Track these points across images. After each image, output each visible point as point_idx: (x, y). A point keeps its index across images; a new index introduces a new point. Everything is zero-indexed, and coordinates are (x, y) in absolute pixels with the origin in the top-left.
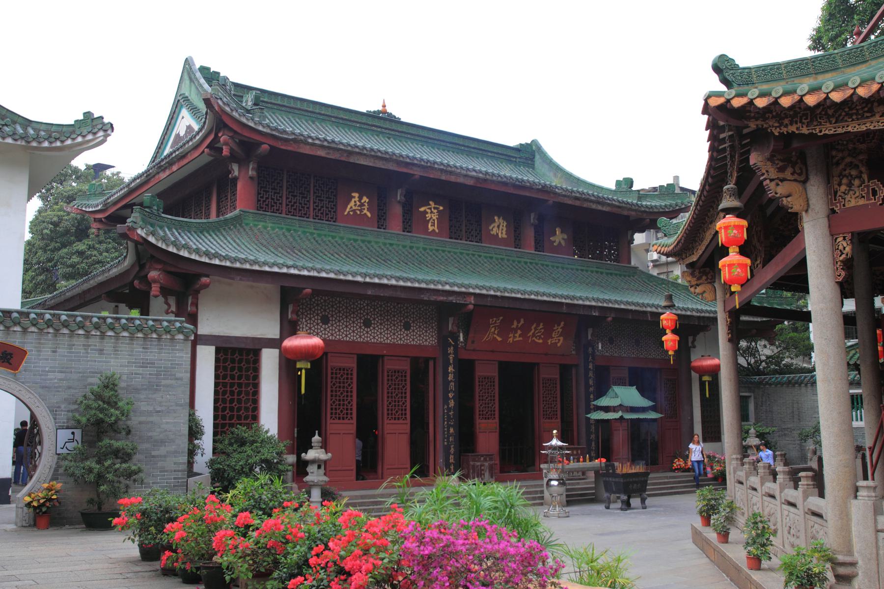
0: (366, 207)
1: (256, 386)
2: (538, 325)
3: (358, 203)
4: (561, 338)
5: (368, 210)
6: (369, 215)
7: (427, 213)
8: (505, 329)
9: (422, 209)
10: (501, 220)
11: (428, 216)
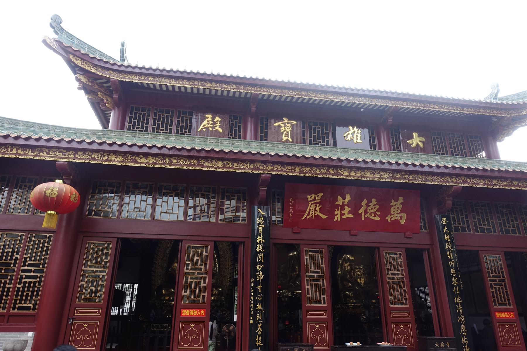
2: (370, 201)
3: (211, 122)
6: (220, 130)
9: (277, 124)
10: (356, 129)
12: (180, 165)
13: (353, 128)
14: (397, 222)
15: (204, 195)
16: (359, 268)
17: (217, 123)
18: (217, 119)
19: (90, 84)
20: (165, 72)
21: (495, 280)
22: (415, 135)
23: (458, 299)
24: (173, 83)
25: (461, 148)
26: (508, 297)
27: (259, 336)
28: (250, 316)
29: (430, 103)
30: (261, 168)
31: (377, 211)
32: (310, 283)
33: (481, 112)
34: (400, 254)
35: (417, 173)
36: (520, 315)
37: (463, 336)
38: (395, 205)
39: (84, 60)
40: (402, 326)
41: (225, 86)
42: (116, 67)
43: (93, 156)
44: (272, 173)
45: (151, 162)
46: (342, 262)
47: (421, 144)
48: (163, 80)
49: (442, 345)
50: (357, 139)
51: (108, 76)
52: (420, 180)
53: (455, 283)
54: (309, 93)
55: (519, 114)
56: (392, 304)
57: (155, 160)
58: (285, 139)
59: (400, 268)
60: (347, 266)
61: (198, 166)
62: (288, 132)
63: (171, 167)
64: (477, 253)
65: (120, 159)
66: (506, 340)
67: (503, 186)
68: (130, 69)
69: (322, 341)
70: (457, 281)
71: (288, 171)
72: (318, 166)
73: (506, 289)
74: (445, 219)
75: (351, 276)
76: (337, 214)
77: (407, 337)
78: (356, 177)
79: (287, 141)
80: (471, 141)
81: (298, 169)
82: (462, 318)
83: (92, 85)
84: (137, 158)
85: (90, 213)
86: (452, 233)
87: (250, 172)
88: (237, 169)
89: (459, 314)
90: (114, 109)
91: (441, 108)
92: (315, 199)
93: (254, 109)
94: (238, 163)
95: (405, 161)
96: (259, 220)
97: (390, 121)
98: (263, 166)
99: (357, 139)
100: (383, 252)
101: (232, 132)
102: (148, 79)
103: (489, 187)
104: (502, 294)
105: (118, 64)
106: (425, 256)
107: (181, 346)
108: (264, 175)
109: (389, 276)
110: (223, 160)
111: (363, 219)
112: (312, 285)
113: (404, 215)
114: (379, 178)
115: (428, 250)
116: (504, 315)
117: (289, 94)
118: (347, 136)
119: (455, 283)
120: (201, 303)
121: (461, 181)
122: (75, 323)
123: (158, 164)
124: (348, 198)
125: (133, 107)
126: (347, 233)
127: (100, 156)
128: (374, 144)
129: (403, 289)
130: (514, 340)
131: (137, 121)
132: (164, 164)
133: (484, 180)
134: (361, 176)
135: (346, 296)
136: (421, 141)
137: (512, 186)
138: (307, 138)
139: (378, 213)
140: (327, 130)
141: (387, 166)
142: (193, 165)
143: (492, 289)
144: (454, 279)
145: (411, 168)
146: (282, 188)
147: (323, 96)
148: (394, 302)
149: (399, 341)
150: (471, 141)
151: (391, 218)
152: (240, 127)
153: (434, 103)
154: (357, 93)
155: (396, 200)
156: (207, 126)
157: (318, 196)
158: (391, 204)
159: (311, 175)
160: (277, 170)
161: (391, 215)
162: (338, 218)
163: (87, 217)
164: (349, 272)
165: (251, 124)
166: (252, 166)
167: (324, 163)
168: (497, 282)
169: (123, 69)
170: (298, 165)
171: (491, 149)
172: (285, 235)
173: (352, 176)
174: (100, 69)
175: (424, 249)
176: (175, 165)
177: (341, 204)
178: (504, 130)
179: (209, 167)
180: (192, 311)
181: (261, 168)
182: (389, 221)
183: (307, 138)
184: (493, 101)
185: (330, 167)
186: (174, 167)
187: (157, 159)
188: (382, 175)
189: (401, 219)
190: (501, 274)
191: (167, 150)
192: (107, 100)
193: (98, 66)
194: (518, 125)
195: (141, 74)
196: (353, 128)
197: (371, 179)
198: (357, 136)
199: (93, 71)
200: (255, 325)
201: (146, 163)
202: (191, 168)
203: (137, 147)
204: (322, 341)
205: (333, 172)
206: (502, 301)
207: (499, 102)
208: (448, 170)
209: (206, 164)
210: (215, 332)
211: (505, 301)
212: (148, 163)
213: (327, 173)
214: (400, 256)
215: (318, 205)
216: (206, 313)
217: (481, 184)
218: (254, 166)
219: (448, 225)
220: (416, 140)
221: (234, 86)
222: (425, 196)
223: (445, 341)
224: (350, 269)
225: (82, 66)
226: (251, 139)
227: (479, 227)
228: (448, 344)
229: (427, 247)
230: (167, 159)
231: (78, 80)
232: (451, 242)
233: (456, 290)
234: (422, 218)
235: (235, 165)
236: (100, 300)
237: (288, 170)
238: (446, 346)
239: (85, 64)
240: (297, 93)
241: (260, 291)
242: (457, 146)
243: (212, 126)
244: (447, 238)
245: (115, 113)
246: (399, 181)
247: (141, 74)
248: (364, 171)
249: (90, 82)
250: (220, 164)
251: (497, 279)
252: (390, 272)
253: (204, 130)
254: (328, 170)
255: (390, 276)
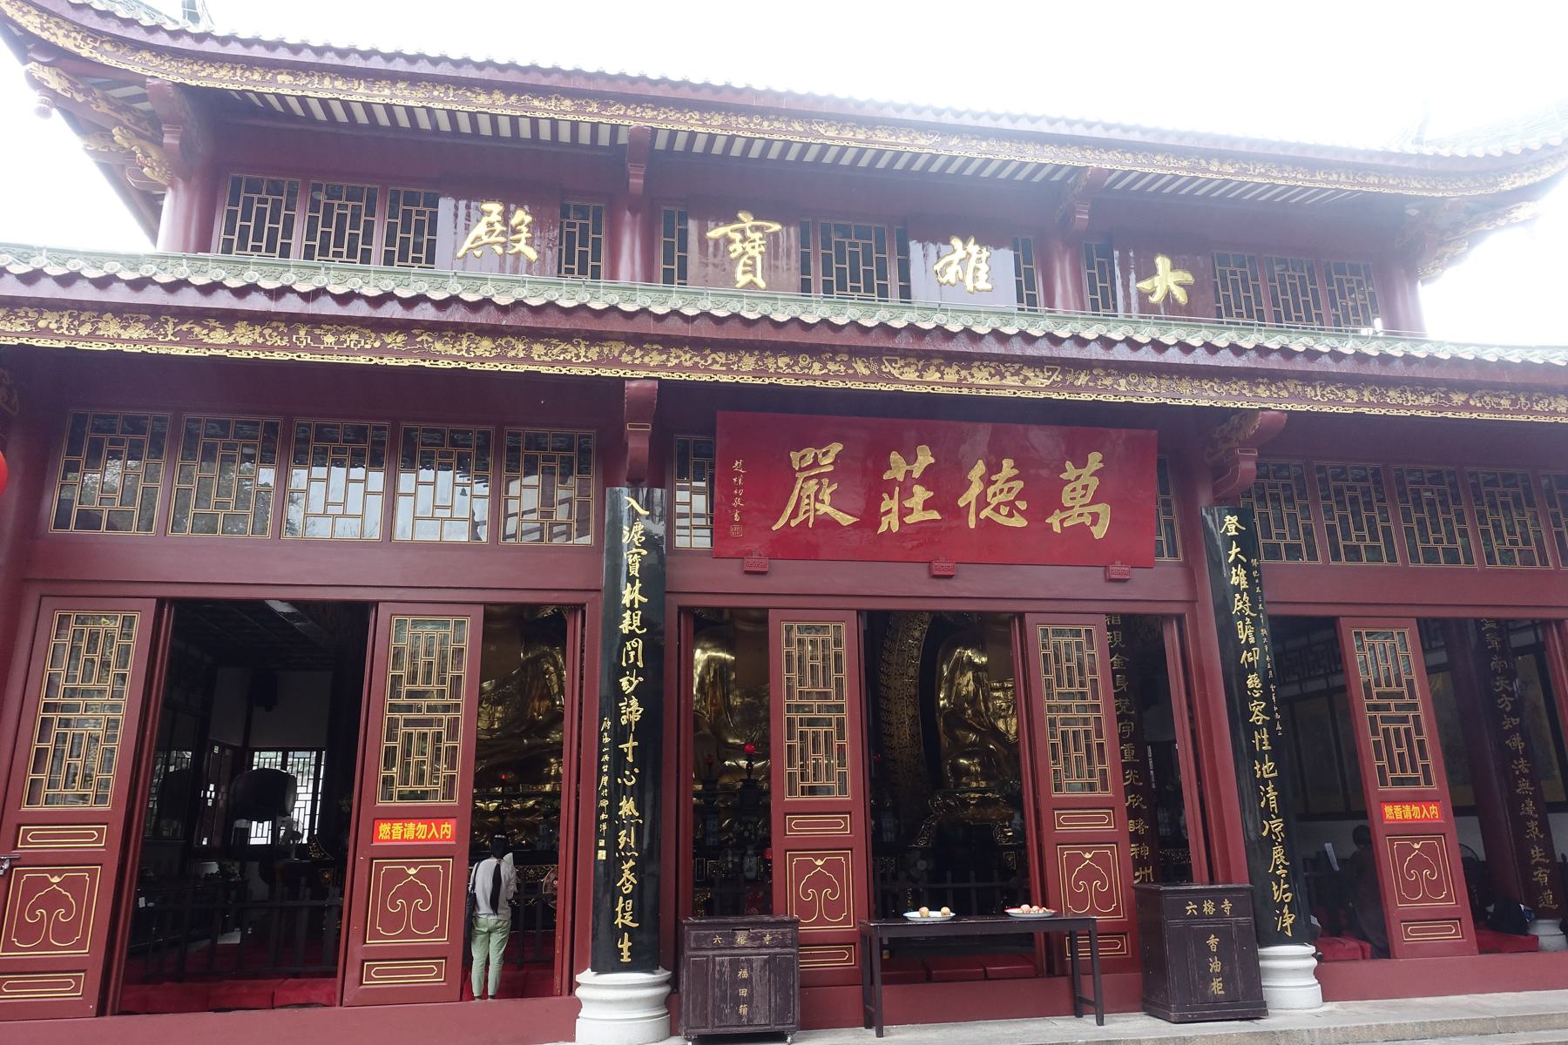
0: (525, 234)
1: (970, 613)
2: (994, 468)
3: (499, 228)
4: (1103, 509)
5: (530, 242)
6: (532, 254)
7: (729, 241)
8: (865, 479)
10: (973, 247)
11: (736, 248)
12: (348, 351)
13: (965, 241)
14: (1082, 531)
15: (450, 455)
16: (1003, 689)
17: (519, 232)
18: (521, 217)
19: (80, 98)
20: (329, 55)
21: (1387, 708)
22: (1162, 263)
23: (1267, 769)
24: (359, 93)
25: (1306, 303)
26: (1423, 757)
27: (626, 897)
28: (599, 835)
29: (1208, 155)
30: (626, 358)
31: (1018, 497)
32: (798, 729)
33: (1368, 185)
34: (1089, 632)
35: (1144, 369)
36: (1459, 811)
37: (1278, 879)
38: (1078, 478)
39: (51, 14)
40: (1088, 856)
41: (536, 103)
42: (161, 40)
43: (42, 324)
44: (663, 375)
45: (249, 342)
46: (952, 672)
47: (1181, 296)
48: (327, 81)
49: (1209, 907)
50: (975, 278)
51: (138, 70)
52: (1150, 393)
53: (1258, 718)
54: (815, 127)
55: (1490, 191)
56: (1058, 788)
57: (262, 335)
58: (742, 279)
59: (1088, 677)
60: (967, 683)
61: (409, 354)
62: (753, 258)
63: (318, 358)
64: (1331, 623)
65: (137, 332)
66: (1413, 889)
67: (1418, 408)
68: (210, 47)
69: (834, 909)
70: (1264, 712)
71: (718, 370)
72: (815, 351)
73: (1419, 732)
74: (1235, 519)
75: (977, 713)
76: (889, 511)
77: (1102, 886)
78: (944, 385)
79: (752, 284)
80: (1340, 282)
81: (749, 363)
82: (1277, 825)
83: (86, 103)
84: (197, 329)
85: (62, 522)
86: (1254, 562)
87: (587, 372)
88: (544, 363)
89: (1266, 814)
90: (173, 185)
91: (1245, 172)
92: (815, 464)
93: (636, 182)
94: (548, 345)
95: (1104, 332)
96: (632, 535)
97: (1081, 224)
98: (632, 353)
99: (975, 278)
100: (1037, 628)
101: (570, 261)
102: (273, 81)
103: (1375, 412)
104: (1405, 749)
105: (170, 26)
106: (1171, 637)
107: (378, 936)
108: (634, 384)
109: (1051, 702)
110: (493, 332)
111: (972, 524)
112: (803, 735)
113: (1103, 509)
114: (1019, 388)
115: (1180, 618)
116: (1409, 812)
117: (749, 129)
118: (943, 272)
119: (1258, 718)
120: (437, 802)
121: (1284, 394)
122: (20, 875)
123: (272, 349)
124: (925, 458)
125: (240, 180)
126: (922, 570)
127: (65, 322)
128: (1030, 289)
129: (1095, 741)
130: (1436, 887)
131: (252, 224)
132: (292, 348)
133: (1359, 392)
134: (959, 384)
135: (959, 771)
136: (1180, 285)
137: (1448, 409)
138: (816, 276)
139: (1022, 505)
140: (881, 250)
141: (1043, 349)
142: (391, 352)
143: (1375, 733)
144: (1257, 708)
145: (1122, 354)
146: (709, 431)
147: (861, 136)
148: (1065, 781)
149: (1079, 900)
150: (1340, 282)
151: (1062, 521)
152: (597, 242)
153: (1222, 157)
154: (973, 123)
155: (1081, 463)
156: (486, 239)
157: (825, 454)
158: (1064, 476)
159: (793, 383)
160: (679, 367)
161: (1063, 509)
162: (890, 523)
163: (52, 530)
164: (973, 700)
165: (633, 233)
166: (593, 353)
167: (837, 340)
168: (1393, 713)
169: (186, 43)
170: (750, 347)
171: (1400, 304)
172: (725, 584)
173: (929, 384)
174: (107, 47)
175: (1166, 617)
176: (330, 351)
177: (901, 477)
178: (1442, 243)
179: (446, 357)
180: (411, 825)
181: (626, 358)
182: (1057, 529)
183: (816, 276)
184: (1411, 149)
185: (855, 352)
186: (328, 359)
187: (267, 332)
188: (1027, 378)
189: (1095, 522)
190: (1405, 688)
191: (299, 300)
192: (147, 156)
193: (101, 33)
194: (1484, 227)
195: (250, 63)
196: (965, 241)
197: (994, 393)
198: (976, 269)
199: (85, 53)
200: (613, 866)
201: (229, 347)
202: (385, 361)
203: (193, 291)
204: (834, 909)
205: (867, 372)
206: (1403, 770)
207: (1428, 151)
208: (1244, 358)
209: (439, 346)
210: (509, 890)
211: (1414, 769)
212: (235, 345)
213: (847, 376)
214: (1090, 641)
215: (825, 481)
216: (457, 834)
217: (1347, 403)
218: (600, 353)
219: (1246, 540)
220: (1167, 279)
221: (568, 102)
222: (1175, 454)
223: (1217, 896)
224: (976, 693)
225: (45, 35)
226: (633, 279)
227: (1341, 544)
228: (1227, 905)
229: (1176, 609)
230: (302, 333)
231: (38, 84)
232: (1250, 592)
233: (1261, 740)
234: (1162, 518)
235: (538, 349)
236: (101, 799)
237: (716, 367)
238: (1219, 912)
239: (54, 29)
240: (776, 124)
241: (630, 759)
242: (1295, 296)
243: (502, 239)
244: (1238, 578)
245: (176, 198)
246: (1084, 397)
247: (250, 63)
248: (969, 368)
249: (79, 91)
250: (485, 346)
251: (1392, 702)
252: (1056, 690)
253: (478, 253)
254: (849, 366)
255: (1055, 702)
